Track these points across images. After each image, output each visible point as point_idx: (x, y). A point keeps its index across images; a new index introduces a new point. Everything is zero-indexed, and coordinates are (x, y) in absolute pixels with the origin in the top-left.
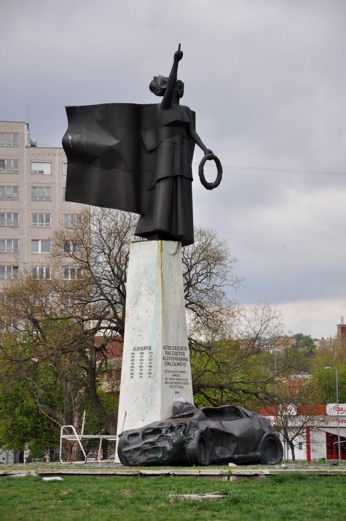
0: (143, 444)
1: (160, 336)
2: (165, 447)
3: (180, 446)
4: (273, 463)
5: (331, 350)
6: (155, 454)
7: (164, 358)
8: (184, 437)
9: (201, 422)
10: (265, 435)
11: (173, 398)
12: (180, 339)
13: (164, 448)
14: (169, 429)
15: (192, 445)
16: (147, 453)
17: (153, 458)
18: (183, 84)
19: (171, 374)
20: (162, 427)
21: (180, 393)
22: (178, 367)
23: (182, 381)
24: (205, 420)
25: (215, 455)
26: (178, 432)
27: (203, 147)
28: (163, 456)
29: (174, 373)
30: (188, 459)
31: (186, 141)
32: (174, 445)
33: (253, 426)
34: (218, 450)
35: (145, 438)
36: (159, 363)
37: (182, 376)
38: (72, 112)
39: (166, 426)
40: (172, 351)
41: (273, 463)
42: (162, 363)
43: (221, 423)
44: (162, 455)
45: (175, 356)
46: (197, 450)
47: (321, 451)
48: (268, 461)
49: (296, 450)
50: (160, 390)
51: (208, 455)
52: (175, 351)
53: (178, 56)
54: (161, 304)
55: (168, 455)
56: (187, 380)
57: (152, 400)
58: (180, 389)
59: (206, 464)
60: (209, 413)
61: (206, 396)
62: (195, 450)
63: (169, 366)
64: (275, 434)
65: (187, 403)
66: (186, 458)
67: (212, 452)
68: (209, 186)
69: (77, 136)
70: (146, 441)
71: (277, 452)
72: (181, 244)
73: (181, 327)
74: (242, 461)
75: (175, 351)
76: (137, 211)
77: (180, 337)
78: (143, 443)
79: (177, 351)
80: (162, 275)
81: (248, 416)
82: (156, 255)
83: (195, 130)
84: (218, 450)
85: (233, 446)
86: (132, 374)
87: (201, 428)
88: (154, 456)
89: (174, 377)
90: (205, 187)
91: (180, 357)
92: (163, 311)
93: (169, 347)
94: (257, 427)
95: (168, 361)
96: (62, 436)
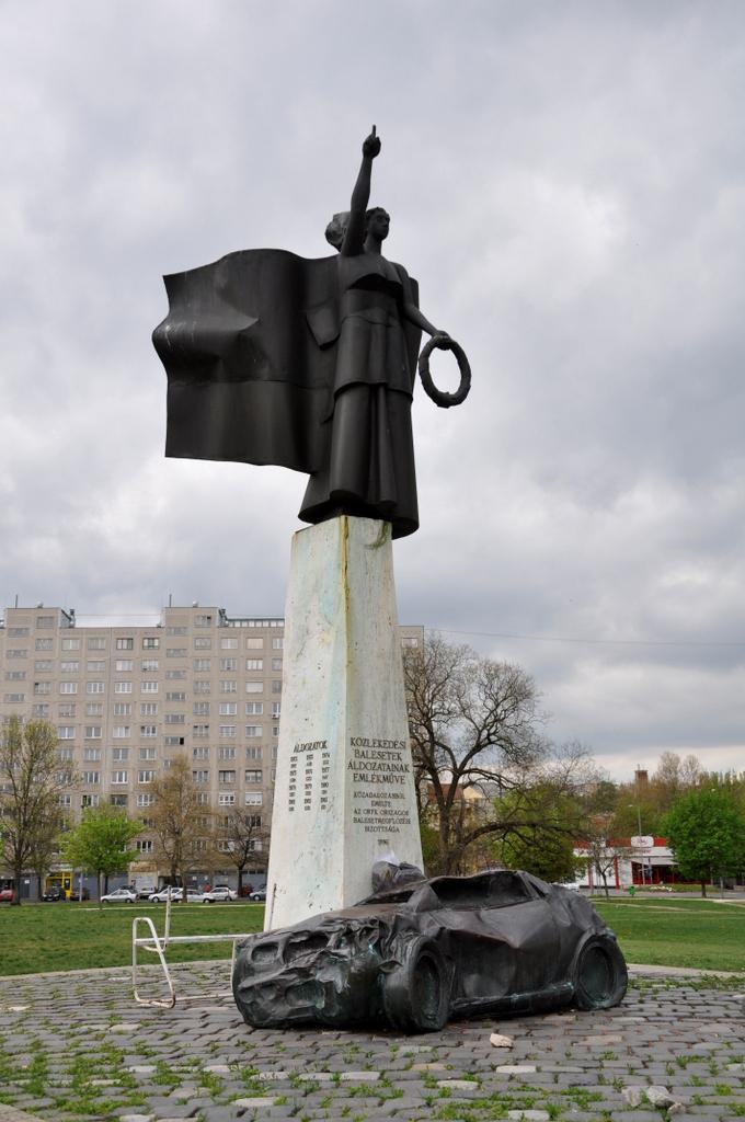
0: (283, 974)
1: (343, 718)
2: (331, 982)
3: (368, 981)
4: (605, 1004)
5: (631, 791)
6: (310, 999)
7: (351, 766)
8: (379, 958)
9: (427, 914)
10: (583, 940)
11: (373, 854)
12: (390, 724)
13: (330, 985)
14: (344, 935)
15: (398, 978)
16: (291, 996)
17: (306, 1009)
18: (382, 210)
19: (369, 800)
20: (329, 929)
21: (390, 842)
22: (387, 785)
23: (395, 817)
24: (438, 908)
25: (465, 995)
26: (362, 945)
27: (431, 331)
28: (328, 1006)
29: (376, 799)
30: (389, 1016)
31: (395, 323)
32: (353, 979)
33: (554, 920)
34: (471, 983)
35: (291, 957)
36: (341, 775)
37: (396, 805)
38: (174, 284)
39: (338, 927)
40: (370, 750)
41: (605, 1004)
42: (347, 776)
43: (478, 917)
44: (326, 1004)
45: (378, 762)
46: (410, 995)
47: (627, 879)
48: (593, 1000)
49: (608, 878)
50: (342, 836)
51: (443, 1001)
52: (377, 750)
53: (372, 148)
54: (345, 649)
55: (339, 1004)
56: (407, 813)
57: (327, 860)
58: (390, 833)
59: (437, 1026)
60: (450, 890)
61: (520, 836)
62: (405, 992)
63: (363, 783)
64: (605, 935)
65: (404, 867)
66: (384, 1013)
67: (455, 988)
68: (443, 401)
69: (179, 325)
70: (291, 966)
71: (612, 976)
72: (390, 528)
73: (392, 698)
74: (531, 1009)
75: (377, 750)
76: (299, 465)
77: (389, 719)
78: (283, 970)
79: (382, 750)
80: (346, 586)
81: (542, 895)
82: (336, 546)
83: (417, 305)
84: (471, 983)
85: (508, 972)
86: (292, 802)
87: (425, 933)
88: (306, 1003)
89: (376, 808)
90: (434, 401)
91: (390, 763)
92: (349, 662)
93: (365, 742)
94: (565, 921)
95: (362, 772)
96: (136, 941)
